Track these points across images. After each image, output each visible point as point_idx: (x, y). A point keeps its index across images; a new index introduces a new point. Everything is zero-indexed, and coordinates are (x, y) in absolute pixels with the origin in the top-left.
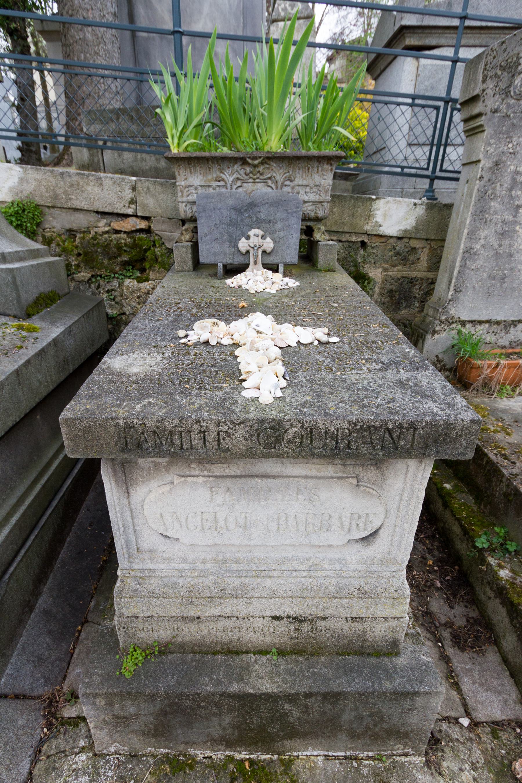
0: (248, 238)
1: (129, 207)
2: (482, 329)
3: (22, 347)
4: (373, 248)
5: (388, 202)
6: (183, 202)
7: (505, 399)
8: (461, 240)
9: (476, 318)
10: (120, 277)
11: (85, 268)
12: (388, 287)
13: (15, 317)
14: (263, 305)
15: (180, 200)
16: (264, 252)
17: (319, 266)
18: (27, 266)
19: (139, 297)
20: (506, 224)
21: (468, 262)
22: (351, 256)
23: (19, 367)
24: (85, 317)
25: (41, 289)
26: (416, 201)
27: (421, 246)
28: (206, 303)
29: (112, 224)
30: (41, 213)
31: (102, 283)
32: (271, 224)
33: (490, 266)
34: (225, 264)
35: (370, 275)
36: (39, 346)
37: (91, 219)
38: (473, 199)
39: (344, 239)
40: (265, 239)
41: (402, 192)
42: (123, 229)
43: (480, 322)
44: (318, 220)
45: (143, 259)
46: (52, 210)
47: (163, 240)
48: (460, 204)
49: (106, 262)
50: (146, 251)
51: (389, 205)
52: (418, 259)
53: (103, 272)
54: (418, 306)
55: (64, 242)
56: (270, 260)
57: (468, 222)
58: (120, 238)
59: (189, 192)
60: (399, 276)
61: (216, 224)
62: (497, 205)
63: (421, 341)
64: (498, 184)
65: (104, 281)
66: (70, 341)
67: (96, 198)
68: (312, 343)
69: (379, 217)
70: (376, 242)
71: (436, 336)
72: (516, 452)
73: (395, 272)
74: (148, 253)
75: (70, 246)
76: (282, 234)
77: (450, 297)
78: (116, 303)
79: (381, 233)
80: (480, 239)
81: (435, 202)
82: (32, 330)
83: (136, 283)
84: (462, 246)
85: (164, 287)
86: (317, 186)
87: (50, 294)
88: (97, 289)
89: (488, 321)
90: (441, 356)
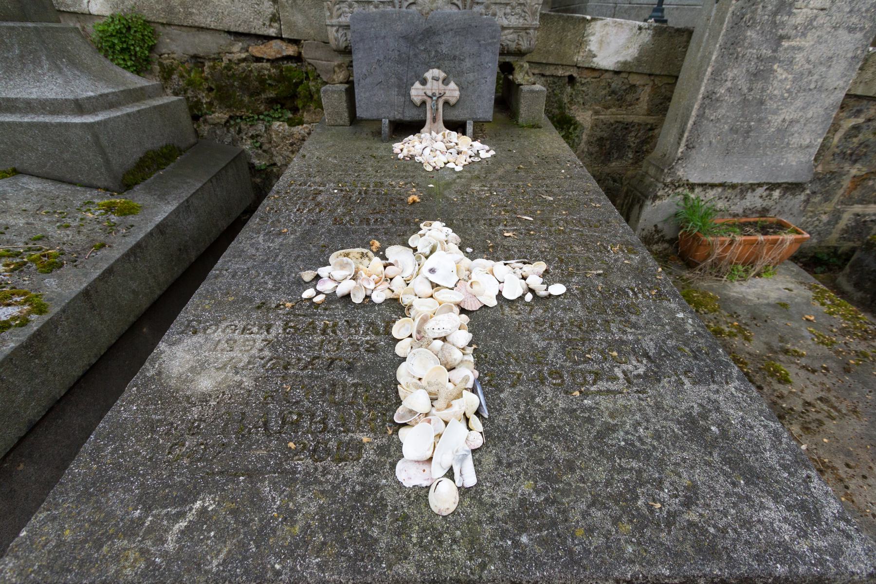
0: (424, 82)
1: (270, 26)
2: (711, 193)
3: (103, 246)
4: (583, 84)
5: (606, 25)
6: (332, 26)
7: (736, 283)
8: (702, 81)
9: (708, 180)
10: (267, 119)
11: (220, 108)
12: (599, 134)
13: (107, 189)
14: (444, 197)
15: (328, 22)
16: (446, 103)
17: (520, 120)
18: (118, 117)
19: (292, 144)
20: (762, 61)
21: (707, 111)
22: (555, 95)
23: (89, 285)
24: (214, 181)
25: (148, 146)
26: (642, 24)
27: (642, 83)
28: (360, 193)
29: (250, 49)
30: (154, 32)
31: (243, 126)
32: (457, 62)
33: (734, 116)
34: (392, 119)
35: (578, 119)
36: (131, 241)
37: (222, 42)
38: (725, 26)
39: (548, 73)
40: (447, 84)
41: (615, 8)
42: (265, 57)
43: (713, 186)
44: (520, 54)
45: (294, 96)
46: (168, 28)
47: (319, 72)
48: (704, 32)
49: (246, 99)
50: (297, 85)
51: (607, 29)
52: (637, 99)
53: (244, 112)
54: (631, 156)
55: (189, 72)
56: (456, 115)
57: (714, 58)
58: (262, 68)
59: (340, 11)
60: (612, 121)
61: (379, 61)
62: (754, 36)
63: (637, 207)
64: (760, 6)
65: (246, 124)
66: (189, 220)
67: (226, 13)
68: (522, 298)
69: (593, 46)
70: (587, 77)
71: (658, 202)
72: (760, 369)
73: (608, 116)
74: (300, 89)
75: (198, 79)
76: (471, 77)
77: (679, 155)
78: (264, 151)
79: (594, 66)
80: (726, 80)
81: (665, 26)
82: (126, 212)
83: (287, 127)
84: (703, 89)
85: (304, 156)
86: (520, 4)
87: (165, 150)
88: (238, 134)
89: (722, 185)
90: (660, 226)
